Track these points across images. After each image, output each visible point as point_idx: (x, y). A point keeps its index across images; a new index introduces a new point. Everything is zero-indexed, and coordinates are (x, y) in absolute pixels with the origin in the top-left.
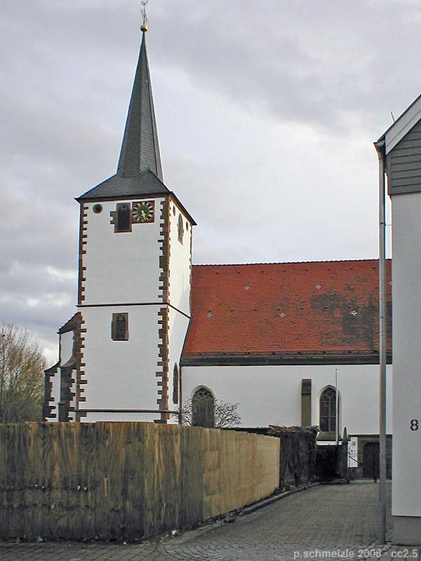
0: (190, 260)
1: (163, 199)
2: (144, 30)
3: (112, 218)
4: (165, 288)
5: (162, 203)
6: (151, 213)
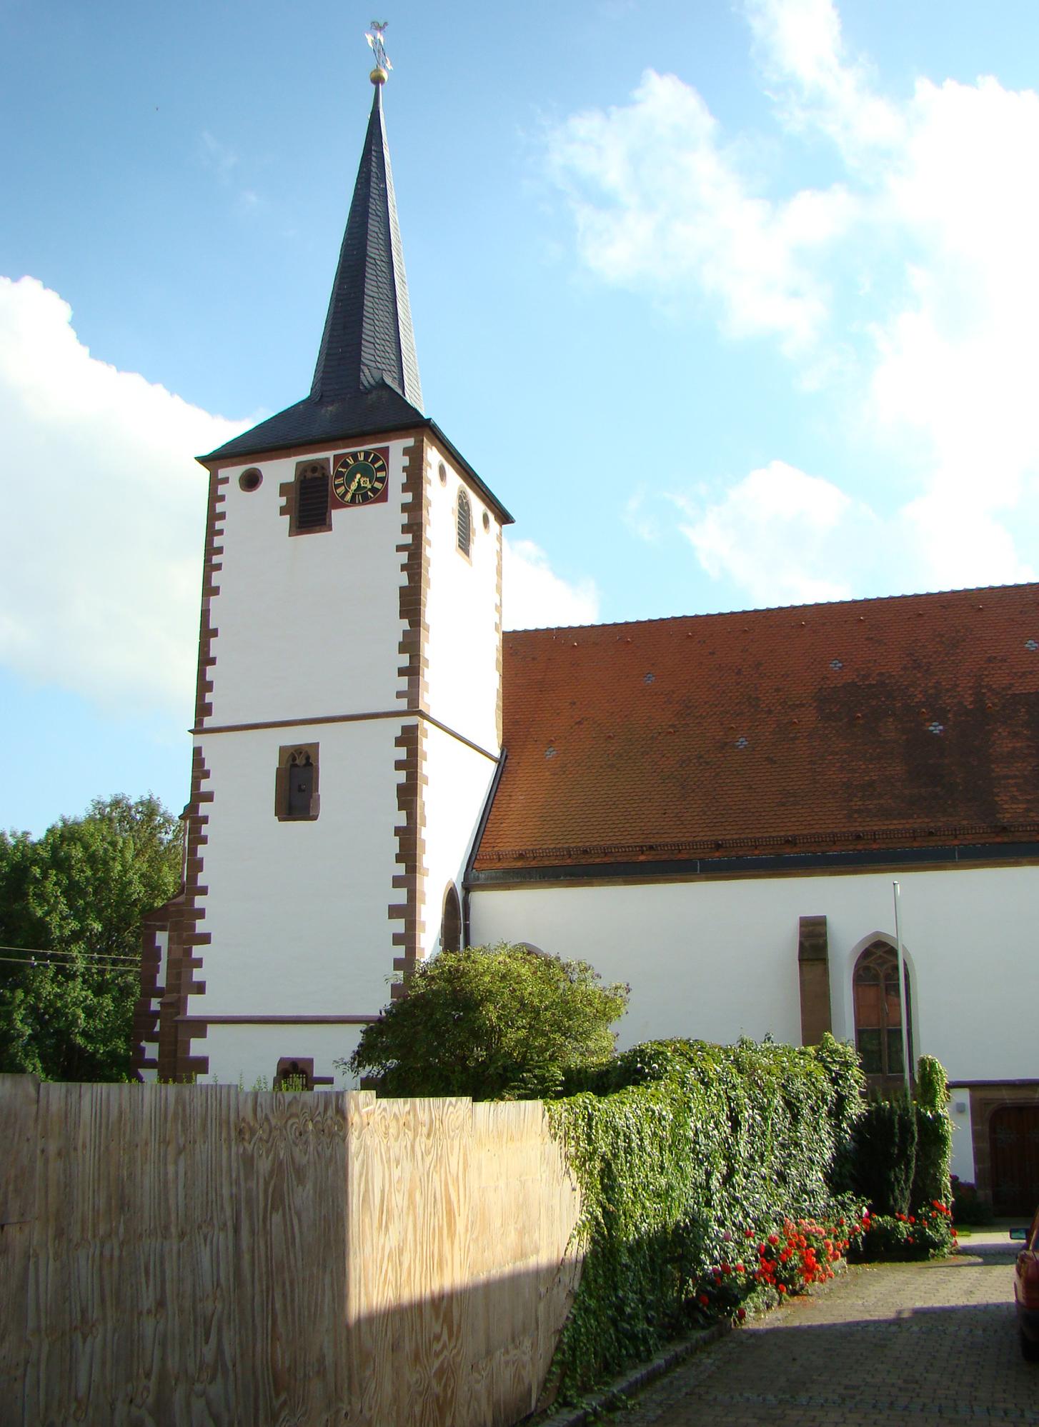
0: (499, 608)
1: (410, 442)
2: (377, 80)
3: (283, 501)
4: (412, 672)
5: (406, 451)
6: (382, 480)
